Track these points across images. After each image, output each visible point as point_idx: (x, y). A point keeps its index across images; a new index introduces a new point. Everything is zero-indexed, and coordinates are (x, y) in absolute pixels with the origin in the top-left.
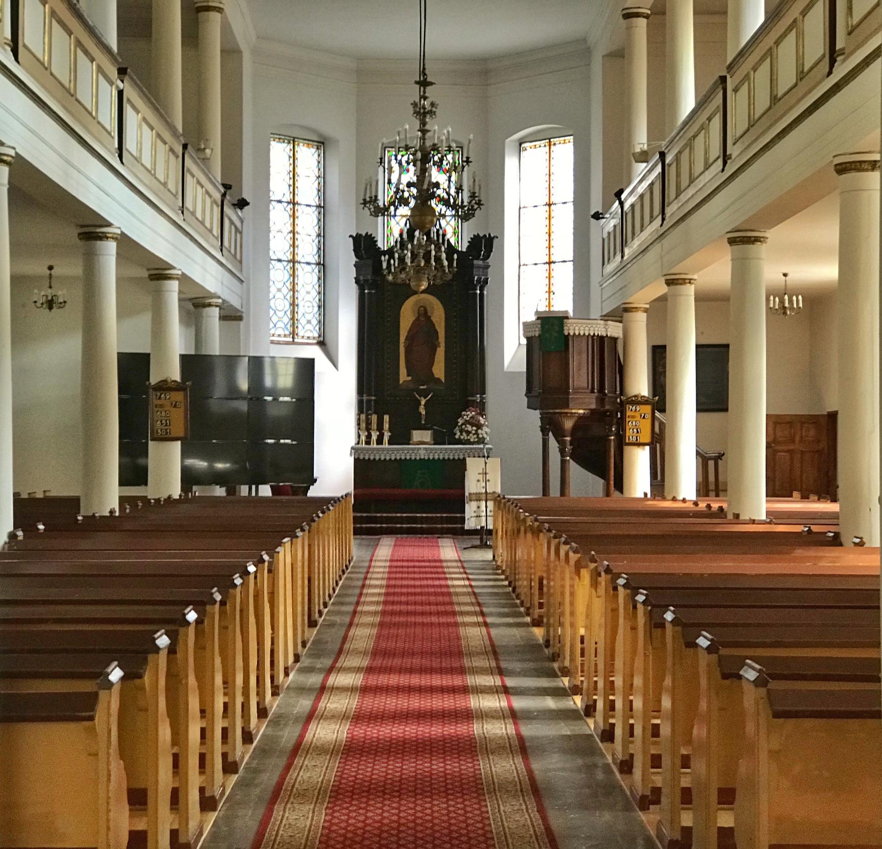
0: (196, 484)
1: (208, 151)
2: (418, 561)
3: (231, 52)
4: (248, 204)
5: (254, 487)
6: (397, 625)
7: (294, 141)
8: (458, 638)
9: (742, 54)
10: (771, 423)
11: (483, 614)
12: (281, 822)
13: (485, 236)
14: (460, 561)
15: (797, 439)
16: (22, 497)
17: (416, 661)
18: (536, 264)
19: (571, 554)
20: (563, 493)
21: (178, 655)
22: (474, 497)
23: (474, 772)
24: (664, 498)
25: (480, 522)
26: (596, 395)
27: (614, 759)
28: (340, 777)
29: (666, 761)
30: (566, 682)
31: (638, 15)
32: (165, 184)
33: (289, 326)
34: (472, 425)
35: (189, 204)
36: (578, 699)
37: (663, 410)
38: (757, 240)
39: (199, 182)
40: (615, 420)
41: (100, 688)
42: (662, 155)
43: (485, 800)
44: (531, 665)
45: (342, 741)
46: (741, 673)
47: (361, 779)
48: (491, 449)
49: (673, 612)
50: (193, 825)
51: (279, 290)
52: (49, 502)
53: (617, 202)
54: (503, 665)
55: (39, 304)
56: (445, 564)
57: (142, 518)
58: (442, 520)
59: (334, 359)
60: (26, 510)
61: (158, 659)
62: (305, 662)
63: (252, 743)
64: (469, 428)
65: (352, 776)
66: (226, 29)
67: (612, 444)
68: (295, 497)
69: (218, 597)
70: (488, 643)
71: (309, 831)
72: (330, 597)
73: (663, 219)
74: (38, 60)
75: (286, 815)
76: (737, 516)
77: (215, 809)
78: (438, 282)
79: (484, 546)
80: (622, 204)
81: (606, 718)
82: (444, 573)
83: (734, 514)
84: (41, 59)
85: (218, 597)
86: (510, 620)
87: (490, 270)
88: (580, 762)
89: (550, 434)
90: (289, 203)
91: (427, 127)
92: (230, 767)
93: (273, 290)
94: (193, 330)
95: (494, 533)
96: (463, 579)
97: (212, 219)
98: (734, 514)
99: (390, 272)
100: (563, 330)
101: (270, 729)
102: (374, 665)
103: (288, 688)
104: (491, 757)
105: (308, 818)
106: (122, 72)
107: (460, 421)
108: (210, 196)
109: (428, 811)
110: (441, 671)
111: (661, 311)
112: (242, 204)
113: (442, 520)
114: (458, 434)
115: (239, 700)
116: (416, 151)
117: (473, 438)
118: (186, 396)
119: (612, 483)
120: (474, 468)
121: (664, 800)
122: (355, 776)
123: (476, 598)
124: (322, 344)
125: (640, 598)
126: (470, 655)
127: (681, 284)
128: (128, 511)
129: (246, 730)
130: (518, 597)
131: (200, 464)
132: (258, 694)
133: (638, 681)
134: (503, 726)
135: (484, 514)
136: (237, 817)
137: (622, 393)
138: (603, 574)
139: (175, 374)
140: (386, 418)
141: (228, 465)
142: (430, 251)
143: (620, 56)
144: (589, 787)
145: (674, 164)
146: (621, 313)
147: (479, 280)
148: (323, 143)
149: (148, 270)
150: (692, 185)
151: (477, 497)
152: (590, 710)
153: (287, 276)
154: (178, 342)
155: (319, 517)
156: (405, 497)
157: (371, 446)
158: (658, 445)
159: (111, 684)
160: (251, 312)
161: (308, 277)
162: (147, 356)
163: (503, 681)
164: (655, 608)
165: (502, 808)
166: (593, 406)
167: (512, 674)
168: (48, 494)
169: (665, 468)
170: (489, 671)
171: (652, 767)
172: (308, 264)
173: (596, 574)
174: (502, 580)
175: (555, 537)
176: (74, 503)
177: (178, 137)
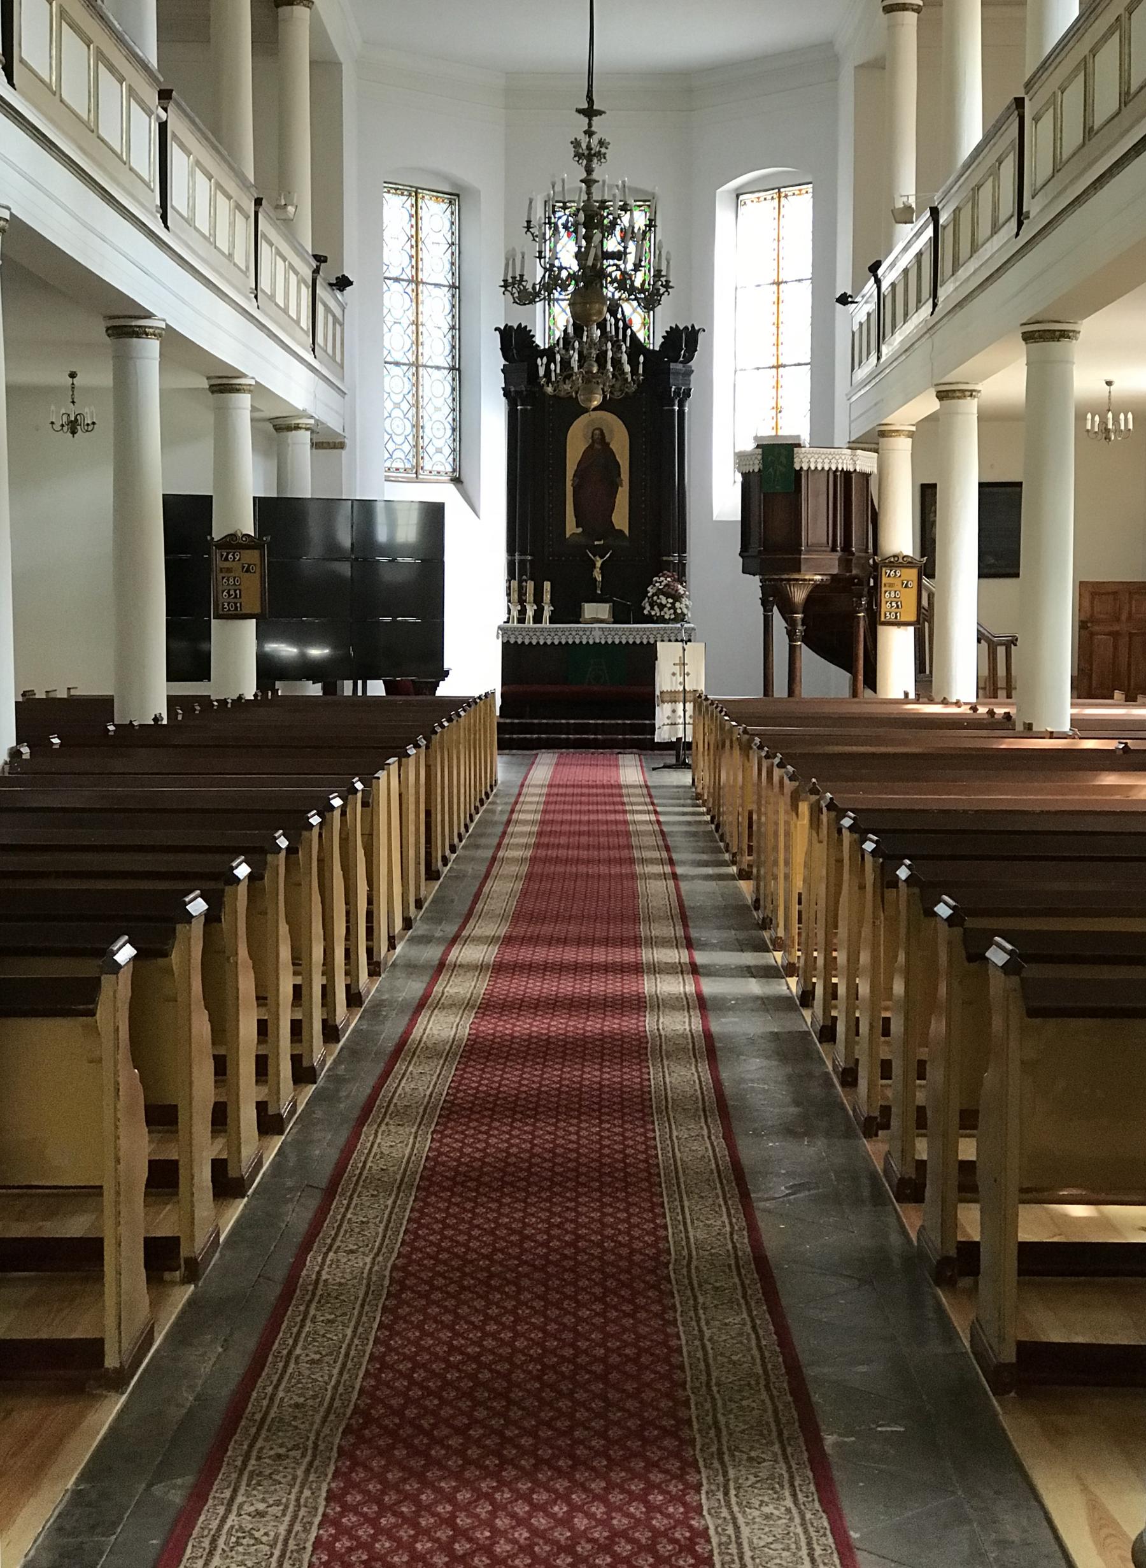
0: (280, 679)
1: (291, 209)
2: (589, 787)
3: (325, 68)
4: (351, 283)
5: (360, 682)
6: (552, 878)
7: (416, 193)
8: (635, 896)
9: (1044, 66)
10: (1087, 596)
11: (671, 862)
12: (370, 1151)
13: (686, 328)
14: (647, 786)
15: (1124, 617)
16: (37, 696)
17: (573, 929)
18: (758, 369)
19: (786, 781)
20: (791, 693)
21: (269, 916)
22: (666, 697)
23: (641, 1083)
24: (931, 701)
25: (676, 732)
26: (839, 554)
27: (835, 1067)
28: (455, 1089)
29: (897, 1069)
30: (778, 957)
31: (904, 7)
32: (230, 256)
33: (410, 457)
34: (668, 596)
35: (265, 284)
36: (793, 982)
37: (931, 576)
38: (1064, 335)
39: (279, 253)
40: (866, 590)
41: (102, 972)
42: (935, 213)
43: (653, 1123)
44: (742, 935)
45: (461, 1040)
46: (987, 954)
47: (484, 1092)
48: (693, 629)
49: (909, 867)
50: (248, 1152)
51: (397, 406)
52: (75, 704)
53: (873, 279)
54: (694, 934)
55: (57, 427)
56: (624, 791)
57: (197, 724)
58: (624, 729)
59: (474, 500)
60: (33, 715)
61: (190, 931)
62: (419, 928)
63: (338, 1041)
64: (663, 600)
65: (473, 1088)
66: (318, 32)
67: (862, 623)
68: (420, 698)
69: (283, 843)
70: (675, 904)
71: (408, 1162)
72: (460, 839)
73: (935, 305)
74: (42, 81)
75: (378, 1141)
76: (1029, 727)
77: (282, 1133)
78: (618, 395)
79: (681, 765)
80: (878, 282)
81: (826, 1008)
82: (623, 804)
83: (1024, 723)
84: (47, 80)
85: (283, 843)
86: (710, 871)
87: (692, 376)
88: (789, 1070)
89: (775, 608)
90: (410, 281)
91: (595, 176)
92: (303, 1074)
93: (389, 405)
94: (275, 462)
95: (694, 745)
96: (649, 812)
97: (299, 305)
98: (1024, 723)
99: (549, 381)
100: (793, 463)
101: (364, 1022)
102: (514, 934)
103: (394, 965)
104: (666, 1063)
105: (407, 1145)
106: (165, 95)
107: (651, 590)
108: (296, 273)
109: (574, 1138)
110: (607, 942)
111: (931, 437)
112: (343, 283)
113: (624, 729)
114: (648, 608)
115: (318, 981)
116: (578, 210)
117: (668, 614)
118: (262, 556)
119: (861, 678)
120: (667, 654)
121: (894, 1123)
122: (476, 1088)
123: (664, 840)
124: (457, 481)
125: (869, 846)
126: (649, 920)
127: (959, 398)
128: (180, 717)
129: (330, 1022)
130: (722, 839)
131: (285, 650)
132: (347, 973)
133: (865, 958)
134: (687, 1020)
135: (681, 721)
136: (311, 1142)
137: (875, 552)
138: (825, 809)
139: (247, 526)
140: (547, 585)
141: (327, 651)
142: (606, 351)
143: (879, 67)
144: (797, 1103)
145: (951, 226)
146: (875, 439)
147: (677, 393)
148: (458, 195)
149: (208, 378)
150: (975, 256)
151: (672, 697)
152: (806, 998)
153: (408, 386)
154: (251, 481)
155: (443, 727)
156: (575, 696)
157: (526, 625)
158: (926, 624)
159: (117, 967)
160: (358, 437)
161: (437, 388)
162: (207, 500)
163: (691, 957)
164: (888, 858)
165: (675, 1133)
166: (835, 571)
167: (704, 946)
168: (73, 692)
169: (935, 661)
170: (675, 943)
171: (882, 1078)
172: (438, 368)
173: (816, 811)
174: (703, 814)
175: (767, 757)
176: (103, 706)
177: (248, 188)
